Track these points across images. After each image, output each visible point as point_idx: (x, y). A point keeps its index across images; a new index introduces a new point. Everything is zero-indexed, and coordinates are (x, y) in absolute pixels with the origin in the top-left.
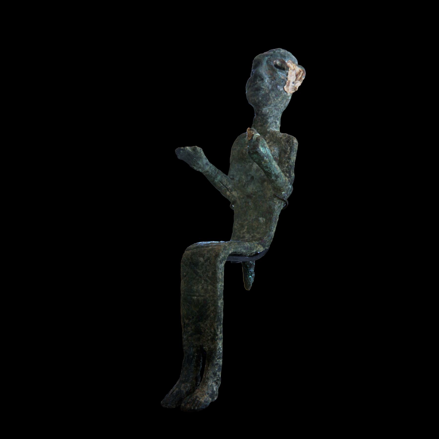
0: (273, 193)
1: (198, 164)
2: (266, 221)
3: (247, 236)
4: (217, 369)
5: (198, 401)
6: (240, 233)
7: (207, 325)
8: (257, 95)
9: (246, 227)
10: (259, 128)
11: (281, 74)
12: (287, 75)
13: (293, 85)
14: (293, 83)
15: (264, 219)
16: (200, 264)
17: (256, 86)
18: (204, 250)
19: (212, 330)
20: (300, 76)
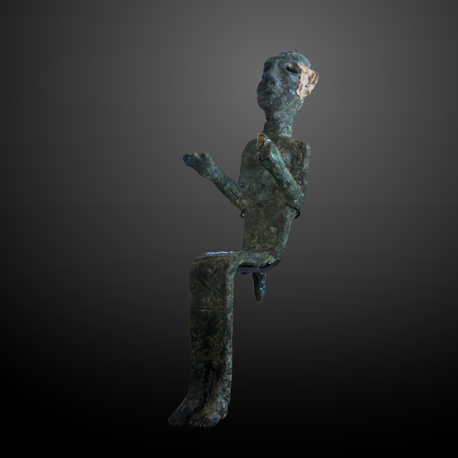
0: (285, 201)
1: (207, 171)
2: (277, 230)
3: (258, 246)
4: (226, 385)
5: (207, 418)
6: (250, 243)
7: (216, 339)
8: (268, 99)
9: (257, 237)
10: (271, 133)
11: (293, 77)
12: (300, 78)
13: (306, 88)
14: (306, 86)
15: (276, 229)
16: (208, 275)
17: (267, 90)
18: (213, 261)
19: (222, 344)
20: (313, 80)
